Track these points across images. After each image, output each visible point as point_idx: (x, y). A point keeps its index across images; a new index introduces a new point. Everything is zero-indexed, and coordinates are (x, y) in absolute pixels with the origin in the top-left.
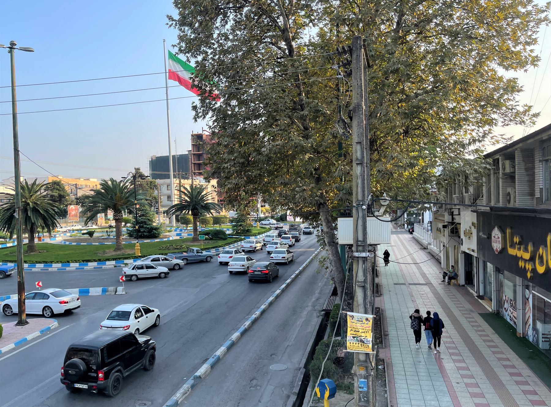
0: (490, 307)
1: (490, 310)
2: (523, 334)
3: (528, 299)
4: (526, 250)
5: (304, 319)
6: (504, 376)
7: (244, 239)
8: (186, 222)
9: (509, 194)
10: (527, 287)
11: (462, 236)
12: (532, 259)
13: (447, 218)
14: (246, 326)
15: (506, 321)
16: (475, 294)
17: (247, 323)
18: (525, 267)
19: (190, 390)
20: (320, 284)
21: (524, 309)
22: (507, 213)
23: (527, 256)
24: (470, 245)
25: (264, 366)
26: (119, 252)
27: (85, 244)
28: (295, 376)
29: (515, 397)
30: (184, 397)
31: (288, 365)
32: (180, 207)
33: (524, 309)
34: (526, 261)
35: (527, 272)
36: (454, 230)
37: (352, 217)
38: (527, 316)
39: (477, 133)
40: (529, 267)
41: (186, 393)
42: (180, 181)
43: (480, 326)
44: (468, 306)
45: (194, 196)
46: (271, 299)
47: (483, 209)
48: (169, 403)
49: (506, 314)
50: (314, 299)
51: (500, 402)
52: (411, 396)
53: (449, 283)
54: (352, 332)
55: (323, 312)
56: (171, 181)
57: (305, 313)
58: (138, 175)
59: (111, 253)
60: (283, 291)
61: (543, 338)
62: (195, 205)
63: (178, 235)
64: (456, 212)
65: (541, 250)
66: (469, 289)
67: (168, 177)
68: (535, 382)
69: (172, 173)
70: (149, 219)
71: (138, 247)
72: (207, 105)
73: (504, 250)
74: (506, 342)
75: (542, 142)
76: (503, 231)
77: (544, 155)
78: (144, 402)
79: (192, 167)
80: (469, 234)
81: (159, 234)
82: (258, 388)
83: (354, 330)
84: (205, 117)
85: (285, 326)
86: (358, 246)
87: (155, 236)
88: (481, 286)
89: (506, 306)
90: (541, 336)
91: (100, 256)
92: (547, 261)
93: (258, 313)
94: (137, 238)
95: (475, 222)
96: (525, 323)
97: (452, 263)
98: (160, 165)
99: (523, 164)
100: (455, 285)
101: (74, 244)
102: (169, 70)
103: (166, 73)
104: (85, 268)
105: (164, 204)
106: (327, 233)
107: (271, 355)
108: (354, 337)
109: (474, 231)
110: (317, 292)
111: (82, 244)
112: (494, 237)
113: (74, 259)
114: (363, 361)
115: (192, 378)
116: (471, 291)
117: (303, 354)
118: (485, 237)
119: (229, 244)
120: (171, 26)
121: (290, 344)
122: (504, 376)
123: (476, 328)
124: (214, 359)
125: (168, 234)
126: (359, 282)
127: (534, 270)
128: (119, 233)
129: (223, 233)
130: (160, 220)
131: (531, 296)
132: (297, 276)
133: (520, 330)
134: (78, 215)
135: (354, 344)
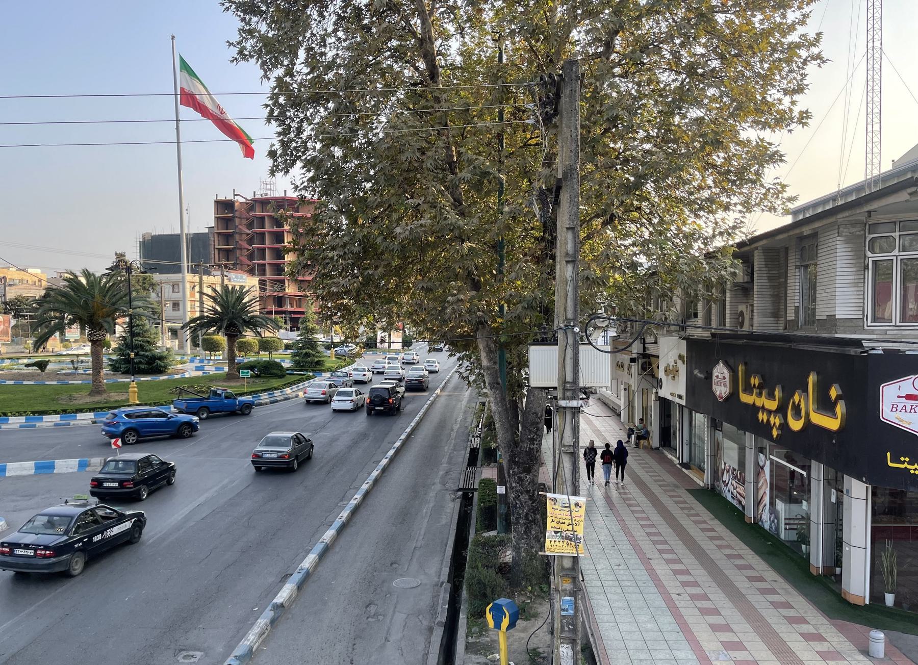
0: (702, 481)
1: (702, 484)
2: (755, 518)
3: (762, 468)
4: (771, 396)
5: (431, 505)
6: (741, 582)
7: (313, 377)
8: (212, 346)
9: (742, 314)
10: (761, 450)
11: (661, 374)
12: (781, 410)
13: (636, 348)
14: (343, 519)
15: (725, 499)
16: (676, 461)
17: (345, 514)
18: (768, 421)
19: (269, 628)
20: (446, 448)
21: (756, 482)
22: (740, 342)
23: (772, 405)
24: (674, 388)
25: (383, 582)
26: (97, 398)
27: (32, 383)
28: (436, 596)
29: (764, 613)
30: (261, 639)
31: (422, 579)
32: (202, 323)
33: (756, 482)
34: (770, 412)
35: (772, 428)
36: (647, 363)
37: (555, 343)
38: (761, 493)
39: (705, 223)
40: (776, 421)
41: (264, 633)
42: (201, 279)
43: (692, 508)
44: (669, 479)
45: (231, 305)
46: (375, 473)
47: (698, 334)
48: (239, 651)
49: (726, 489)
50: (441, 473)
51: (744, 621)
52: (617, 617)
53: (637, 445)
54: (554, 524)
55: (460, 493)
56: (183, 278)
57: (432, 494)
58: (121, 265)
59: (85, 399)
60: (392, 460)
61: (786, 524)
62: (230, 318)
63: (197, 369)
64: (650, 339)
65: (796, 398)
66: (667, 453)
67: (178, 270)
68: (785, 589)
69: (185, 263)
70: (148, 342)
71: (133, 387)
72: (291, 152)
73: (733, 396)
74: (732, 531)
75: (801, 238)
76: (733, 370)
77: (802, 258)
78: (191, 653)
79: (214, 255)
80: (672, 372)
81: (165, 367)
82: (381, 618)
83: (557, 520)
84: (287, 172)
85: (405, 516)
86: (565, 390)
87: (160, 371)
88: (686, 448)
89: (726, 477)
90: (782, 521)
91: (63, 404)
92: (807, 413)
93: (358, 496)
94: (126, 373)
95: (684, 353)
96: (758, 503)
97: (638, 416)
98: (161, 251)
99: (765, 270)
100: (645, 448)
101: (8, 382)
102: (182, 89)
103: (176, 95)
104: (38, 424)
105: (171, 318)
106: (488, 368)
107: (391, 565)
108: (556, 532)
109: (682, 369)
110: (445, 460)
111: (25, 383)
112: (717, 377)
113: (14, 409)
114: (568, 569)
115: (269, 607)
116: (670, 456)
117: (442, 561)
118: (702, 376)
119: (289, 385)
120: (227, 9)
121: (419, 545)
122: (741, 582)
123: (686, 512)
124: (300, 576)
125: (179, 366)
126: (565, 446)
127: (784, 426)
128: (97, 365)
129: (278, 366)
130: (165, 343)
131: (768, 463)
132: (409, 436)
133: (750, 513)
134: (10, 332)
135: (557, 543)
